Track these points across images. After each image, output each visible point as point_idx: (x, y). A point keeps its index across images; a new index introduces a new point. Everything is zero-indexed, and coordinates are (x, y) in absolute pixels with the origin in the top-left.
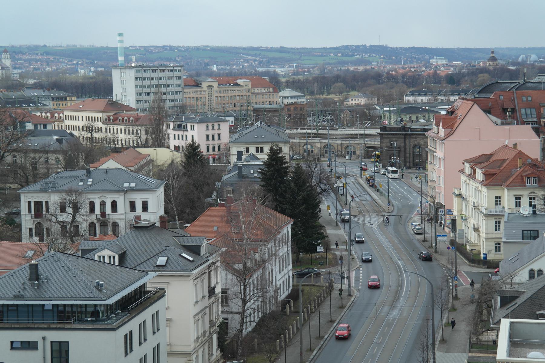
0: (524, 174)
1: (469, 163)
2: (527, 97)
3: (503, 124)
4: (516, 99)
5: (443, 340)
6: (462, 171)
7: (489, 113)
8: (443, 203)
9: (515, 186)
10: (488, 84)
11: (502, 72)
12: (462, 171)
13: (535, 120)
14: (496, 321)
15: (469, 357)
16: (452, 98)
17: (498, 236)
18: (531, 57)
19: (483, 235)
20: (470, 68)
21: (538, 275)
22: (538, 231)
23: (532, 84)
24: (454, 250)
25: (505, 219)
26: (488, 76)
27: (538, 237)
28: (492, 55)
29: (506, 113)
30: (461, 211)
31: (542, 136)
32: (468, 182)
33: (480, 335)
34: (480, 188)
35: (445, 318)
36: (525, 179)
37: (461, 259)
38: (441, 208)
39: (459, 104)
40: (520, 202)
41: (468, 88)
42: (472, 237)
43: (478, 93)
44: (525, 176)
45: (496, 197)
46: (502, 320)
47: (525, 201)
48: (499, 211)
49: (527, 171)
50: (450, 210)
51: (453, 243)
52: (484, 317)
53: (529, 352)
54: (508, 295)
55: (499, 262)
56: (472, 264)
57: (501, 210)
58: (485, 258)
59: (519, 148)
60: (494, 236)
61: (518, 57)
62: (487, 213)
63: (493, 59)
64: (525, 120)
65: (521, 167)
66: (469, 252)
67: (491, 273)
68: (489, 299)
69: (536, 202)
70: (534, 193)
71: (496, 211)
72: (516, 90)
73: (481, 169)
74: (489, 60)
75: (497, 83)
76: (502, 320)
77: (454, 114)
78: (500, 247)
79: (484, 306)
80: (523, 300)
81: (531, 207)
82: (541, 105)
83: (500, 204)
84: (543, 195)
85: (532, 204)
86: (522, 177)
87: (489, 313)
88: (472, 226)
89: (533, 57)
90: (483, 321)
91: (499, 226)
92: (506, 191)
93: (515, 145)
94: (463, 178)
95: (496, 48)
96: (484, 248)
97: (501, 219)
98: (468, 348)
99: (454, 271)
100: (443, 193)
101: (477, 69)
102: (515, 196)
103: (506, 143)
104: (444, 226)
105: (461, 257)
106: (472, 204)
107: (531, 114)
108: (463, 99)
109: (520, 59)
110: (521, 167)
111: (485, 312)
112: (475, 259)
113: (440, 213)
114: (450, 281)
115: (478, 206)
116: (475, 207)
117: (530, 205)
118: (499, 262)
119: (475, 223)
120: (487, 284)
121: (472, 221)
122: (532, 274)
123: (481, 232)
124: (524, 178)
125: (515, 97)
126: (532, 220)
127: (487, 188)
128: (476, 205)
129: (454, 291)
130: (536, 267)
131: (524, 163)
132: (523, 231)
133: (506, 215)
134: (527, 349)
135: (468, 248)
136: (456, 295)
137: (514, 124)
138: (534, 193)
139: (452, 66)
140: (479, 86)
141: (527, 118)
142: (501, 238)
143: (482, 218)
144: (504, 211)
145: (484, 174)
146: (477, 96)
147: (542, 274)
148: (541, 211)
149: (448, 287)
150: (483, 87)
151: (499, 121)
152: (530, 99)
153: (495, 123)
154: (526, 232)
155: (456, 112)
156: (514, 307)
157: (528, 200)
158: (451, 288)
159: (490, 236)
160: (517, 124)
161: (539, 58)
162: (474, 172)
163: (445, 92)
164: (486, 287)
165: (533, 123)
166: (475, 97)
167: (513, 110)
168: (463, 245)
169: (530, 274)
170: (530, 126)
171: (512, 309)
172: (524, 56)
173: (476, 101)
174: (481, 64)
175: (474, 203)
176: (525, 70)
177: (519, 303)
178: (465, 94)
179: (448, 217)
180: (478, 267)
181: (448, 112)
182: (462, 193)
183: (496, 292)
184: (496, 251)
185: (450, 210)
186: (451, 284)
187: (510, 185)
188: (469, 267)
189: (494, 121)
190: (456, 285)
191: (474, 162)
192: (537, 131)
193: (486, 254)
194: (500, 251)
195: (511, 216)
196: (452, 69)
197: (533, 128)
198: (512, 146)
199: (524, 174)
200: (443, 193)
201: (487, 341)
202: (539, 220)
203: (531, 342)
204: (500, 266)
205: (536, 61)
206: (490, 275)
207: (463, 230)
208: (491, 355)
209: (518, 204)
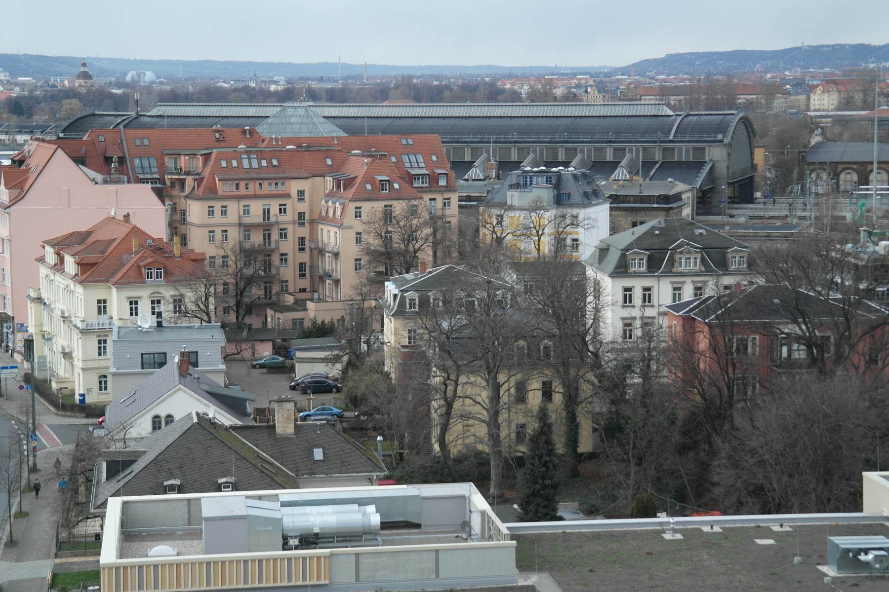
0: (142, 264)
1: (53, 246)
2: (142, 139)
3: (105, 182)
4: (124, 143)
5: (12, 541)
6: (41, 260)
7: (82, 164)
8: (10, 314)
9: (128, 283)
10: (79, 116)
11: (100, 97)
12: (41, 260)
13: (157, 176)
14: (99, 503)
15: (56, 565)
16: (20, 138)
17: (103, 364)
18: (145, 74)
19: (79, 364)
20: (48, 88)
21: (167, 423)
22: (197, 353)
23: (149, 119)
24: (30, 391)
25: (113, 336)
26: (79, 104)
27: (165, 363)
28: (82, 69)
29: (110, 164)
30: (41, 325)
31: (167, 202)
32: (52, 277)
33: (73, 527)
34: (72, 288)
35: (16, 504)
36: (144, 272)
37: (42, 404)
38: (6, 322)
39: (32, 148)
40: (136, 309)
41: (46, 121)
42: (61, 368)
43: (63, 131)
44: (145, 266)
45: (99, 301)
46: (110, 499)
47: (145, 307)
48: (105, 324)
49: (147, 257)
50: (22, 325)
51: (28, 378)
52: (80, 497)
53: (151, 548)
54: (120, 459)
55: (105, 406)
56: (60, 413)
57: (108, 321)
58: (82, 401)
59: (134, 221)
60: (96, 365)
61: (126, 74)
62: (84, 327)
63: (86, 76)
64: (141, 176)
65: (136, 252)
66: (56, 392)
67: (92, 425)
68: (88, 467)
69: (162, 308)
70: (158, 293)
71: (99, 324)
72: (124, 127)
73: (73, 255)
74: (78, 77)
75: (94, 115)
76: (110, 499)
77: (25, 164)
78: (106, 382)
79: (81, 479)
80: (144, 465)
81: (155, 316)
82: (165, 152)
83: (105, 312)
84: (172, 296)
85: (156, 310)
86: (139, 267)
87: (88, 490)
88: (61, 350)
89: (149, 76)
90: (78, 503)
91: (105, 348)
92: (114, 290)
93: (127, 216)
94: (43, 271)
95: (88, 58)
96: (81, 385)
97: (107, 336)
98: (54, 550)
99: (31, 425)
100: (9, 297)
101: (60, 91)
102: (129, 298)
103: (113, 214)
104: (13, 351)
105: (42, 401)
106: (59, 313)
107: (150, 167)
108: (37, 139)
109: (128, 78)
110: (136, 252)
111: (82, 489)
112: (65, 404)
113: (5, 330)
114: (25, 442)
115: (70, 317)
116: (65, 318)
117: (153, 313)
118: (105, 406)
119: (65, 344)
120: (86, 444)
121: (60, 342)
122: (156, 423)
123: (76, 359)
124: (143, 269)
125: (124, 139)
126: (157, 336)
127: (84, 287)
128: (66, 315)
129: (31, 458)
130: (162, 411)
131: (141, 246)
132: (142, 354)
133: (115, 330)
134: (149, 543)
135: (54, 386)
136: (35, 464)
137: (124, 182)
138: (158, 293)
139: (16, 84)
140: (65, 119)
141: (143, 173)
142: (108, 368)
143: (76, 336)
144: (111, 324)
145: (78, 264)
146: (61, 135)
147: (172, 421)
148: (170, 322)
149: (21, 452)
150: (71, 121)
151: (99, 177)
152: (146, 142)
153: (93, 180)
154: (147, 356)
155: (28, 161)
156: (130, 477)
157: (150, 305)
158: (26, 453)
159: (90, 365)
160: (128, 182)
161: (158, 77)
162: (62, 260)
163: (8, 127)
164: (84, 448)
165: (153, 181)
166: (59, 138)
167: (122, 160)
168: (45, 381)
169: (154, 423)
170: (149, 186)
171: (126, 480)
172: (135, 73)
173: (60, 143)
174: (66, 82)
175: (62, 312)
176: (137, 96)
177: (136, 471)
178: (42, 132)
179: (20, 336)
180: (71, 417)
181: (13, 161)
182: (43, 296)
183: (100, 455)
184: (101, 389)
185: (22, 325)
186: (25, 447)
187: (121, 282)
188: (56, 417)
189: (92, 177)
190: (35, 449)
191: (61, 245)
192: (160, 194)
193: (83, 395)
194: (106, 388)
195: (123, 331)
196: (17, 89)
197: (152, 188)
198: (122, 219)
199: (142, 264)
200: (9, 297)
201: (85, 536)
202: (167, 335)
203: (155, 531)
204: (107, 414)
205: (153, 82)
206: (91, 429)
207: (45, 357)
208: (91, 559)
209: (134, 312)
